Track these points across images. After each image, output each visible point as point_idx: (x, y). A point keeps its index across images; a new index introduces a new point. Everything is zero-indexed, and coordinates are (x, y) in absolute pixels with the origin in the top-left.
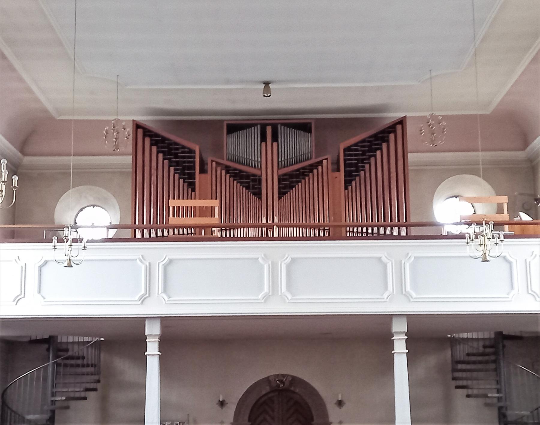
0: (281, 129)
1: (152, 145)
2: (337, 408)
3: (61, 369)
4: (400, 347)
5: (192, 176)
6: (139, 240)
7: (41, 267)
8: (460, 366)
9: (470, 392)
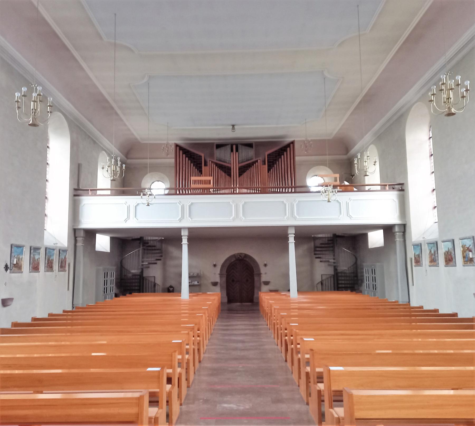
0: (240, 147)
1: (183, 154)
2: (264, 267)
3: (146, 251)
4: (292, 240)
5: (201, 167)
6: (178, 195)
7: (136, 207)
8: (317, 249)
9: (322, 260)
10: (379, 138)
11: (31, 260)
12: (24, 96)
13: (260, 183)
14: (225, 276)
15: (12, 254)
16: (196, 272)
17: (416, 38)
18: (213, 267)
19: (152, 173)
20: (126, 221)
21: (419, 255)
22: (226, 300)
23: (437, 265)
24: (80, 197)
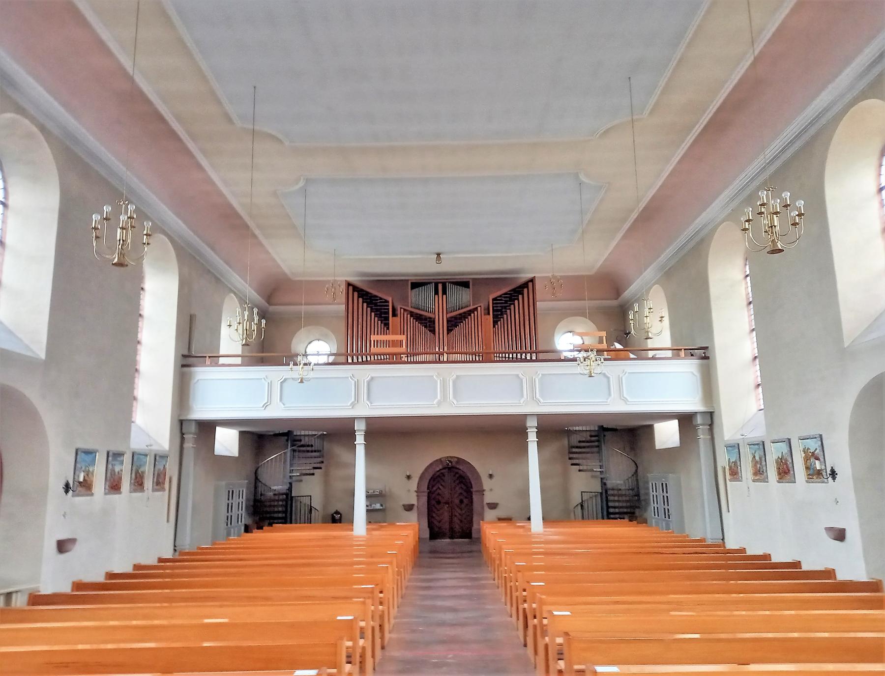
1: (359, 297)
4: (532, 437)
5: (387, 319)
6: (350, 364)
8: (574, 450)
10: (668, 275)
11: (109, 474)
12: (106, 219)
13: (480, 343)
15: (78, 465)
16: (377, 487)
17: (718, 125)
19: (309, 327)
20: (265, 406)
21: (735, 463)
22: (427, 535)
23: (765, 480)
24: (193, 369)
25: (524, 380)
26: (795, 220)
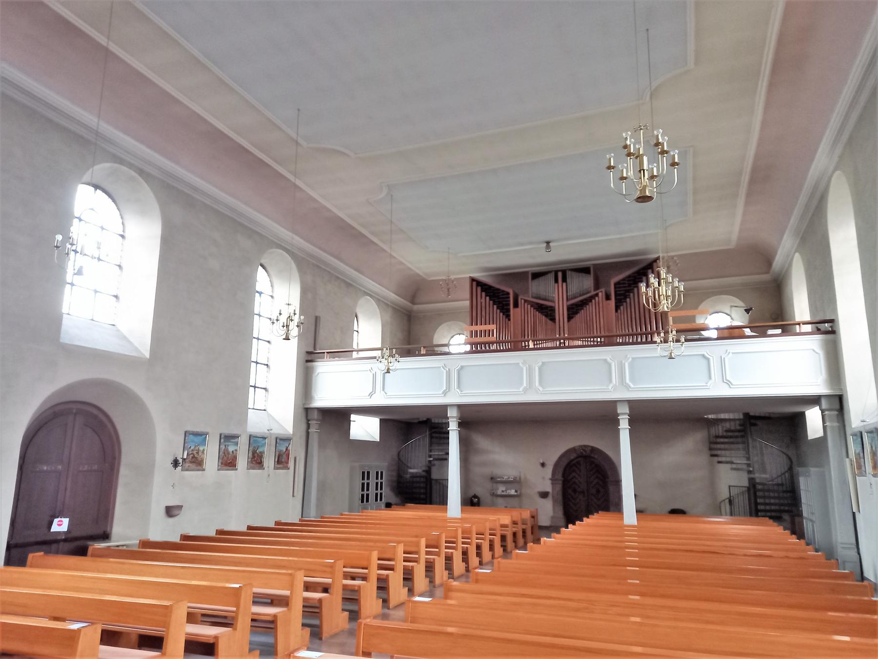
0: (569, 273)
1: (482, 291)
4: (624, 424)
5: (508, 310)
9: (720, 459)
14: (561, 482)
18: (540, 467)
20: (371, 395)
25: (613, 365)
26: (658, 139)
